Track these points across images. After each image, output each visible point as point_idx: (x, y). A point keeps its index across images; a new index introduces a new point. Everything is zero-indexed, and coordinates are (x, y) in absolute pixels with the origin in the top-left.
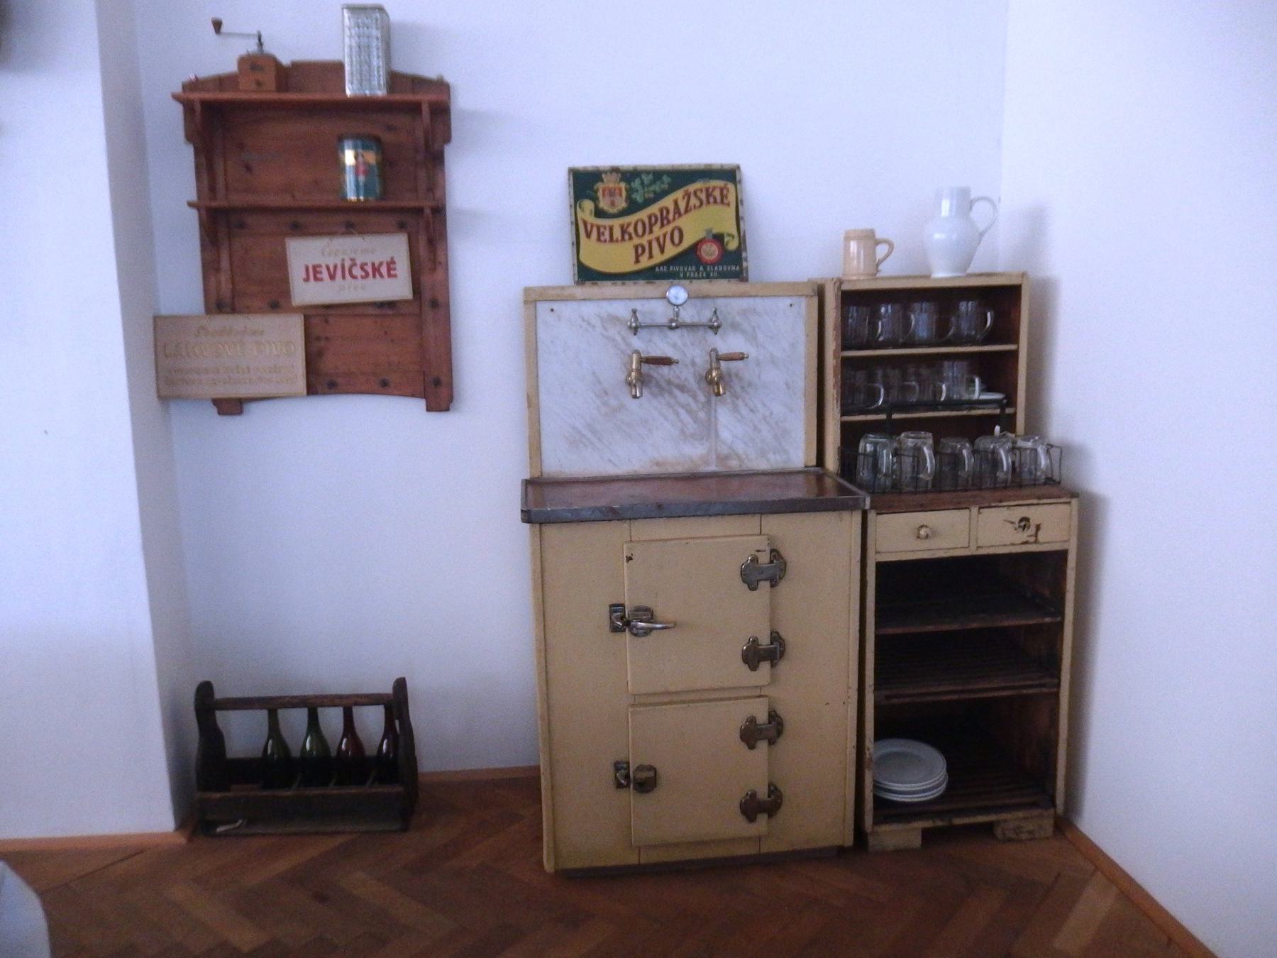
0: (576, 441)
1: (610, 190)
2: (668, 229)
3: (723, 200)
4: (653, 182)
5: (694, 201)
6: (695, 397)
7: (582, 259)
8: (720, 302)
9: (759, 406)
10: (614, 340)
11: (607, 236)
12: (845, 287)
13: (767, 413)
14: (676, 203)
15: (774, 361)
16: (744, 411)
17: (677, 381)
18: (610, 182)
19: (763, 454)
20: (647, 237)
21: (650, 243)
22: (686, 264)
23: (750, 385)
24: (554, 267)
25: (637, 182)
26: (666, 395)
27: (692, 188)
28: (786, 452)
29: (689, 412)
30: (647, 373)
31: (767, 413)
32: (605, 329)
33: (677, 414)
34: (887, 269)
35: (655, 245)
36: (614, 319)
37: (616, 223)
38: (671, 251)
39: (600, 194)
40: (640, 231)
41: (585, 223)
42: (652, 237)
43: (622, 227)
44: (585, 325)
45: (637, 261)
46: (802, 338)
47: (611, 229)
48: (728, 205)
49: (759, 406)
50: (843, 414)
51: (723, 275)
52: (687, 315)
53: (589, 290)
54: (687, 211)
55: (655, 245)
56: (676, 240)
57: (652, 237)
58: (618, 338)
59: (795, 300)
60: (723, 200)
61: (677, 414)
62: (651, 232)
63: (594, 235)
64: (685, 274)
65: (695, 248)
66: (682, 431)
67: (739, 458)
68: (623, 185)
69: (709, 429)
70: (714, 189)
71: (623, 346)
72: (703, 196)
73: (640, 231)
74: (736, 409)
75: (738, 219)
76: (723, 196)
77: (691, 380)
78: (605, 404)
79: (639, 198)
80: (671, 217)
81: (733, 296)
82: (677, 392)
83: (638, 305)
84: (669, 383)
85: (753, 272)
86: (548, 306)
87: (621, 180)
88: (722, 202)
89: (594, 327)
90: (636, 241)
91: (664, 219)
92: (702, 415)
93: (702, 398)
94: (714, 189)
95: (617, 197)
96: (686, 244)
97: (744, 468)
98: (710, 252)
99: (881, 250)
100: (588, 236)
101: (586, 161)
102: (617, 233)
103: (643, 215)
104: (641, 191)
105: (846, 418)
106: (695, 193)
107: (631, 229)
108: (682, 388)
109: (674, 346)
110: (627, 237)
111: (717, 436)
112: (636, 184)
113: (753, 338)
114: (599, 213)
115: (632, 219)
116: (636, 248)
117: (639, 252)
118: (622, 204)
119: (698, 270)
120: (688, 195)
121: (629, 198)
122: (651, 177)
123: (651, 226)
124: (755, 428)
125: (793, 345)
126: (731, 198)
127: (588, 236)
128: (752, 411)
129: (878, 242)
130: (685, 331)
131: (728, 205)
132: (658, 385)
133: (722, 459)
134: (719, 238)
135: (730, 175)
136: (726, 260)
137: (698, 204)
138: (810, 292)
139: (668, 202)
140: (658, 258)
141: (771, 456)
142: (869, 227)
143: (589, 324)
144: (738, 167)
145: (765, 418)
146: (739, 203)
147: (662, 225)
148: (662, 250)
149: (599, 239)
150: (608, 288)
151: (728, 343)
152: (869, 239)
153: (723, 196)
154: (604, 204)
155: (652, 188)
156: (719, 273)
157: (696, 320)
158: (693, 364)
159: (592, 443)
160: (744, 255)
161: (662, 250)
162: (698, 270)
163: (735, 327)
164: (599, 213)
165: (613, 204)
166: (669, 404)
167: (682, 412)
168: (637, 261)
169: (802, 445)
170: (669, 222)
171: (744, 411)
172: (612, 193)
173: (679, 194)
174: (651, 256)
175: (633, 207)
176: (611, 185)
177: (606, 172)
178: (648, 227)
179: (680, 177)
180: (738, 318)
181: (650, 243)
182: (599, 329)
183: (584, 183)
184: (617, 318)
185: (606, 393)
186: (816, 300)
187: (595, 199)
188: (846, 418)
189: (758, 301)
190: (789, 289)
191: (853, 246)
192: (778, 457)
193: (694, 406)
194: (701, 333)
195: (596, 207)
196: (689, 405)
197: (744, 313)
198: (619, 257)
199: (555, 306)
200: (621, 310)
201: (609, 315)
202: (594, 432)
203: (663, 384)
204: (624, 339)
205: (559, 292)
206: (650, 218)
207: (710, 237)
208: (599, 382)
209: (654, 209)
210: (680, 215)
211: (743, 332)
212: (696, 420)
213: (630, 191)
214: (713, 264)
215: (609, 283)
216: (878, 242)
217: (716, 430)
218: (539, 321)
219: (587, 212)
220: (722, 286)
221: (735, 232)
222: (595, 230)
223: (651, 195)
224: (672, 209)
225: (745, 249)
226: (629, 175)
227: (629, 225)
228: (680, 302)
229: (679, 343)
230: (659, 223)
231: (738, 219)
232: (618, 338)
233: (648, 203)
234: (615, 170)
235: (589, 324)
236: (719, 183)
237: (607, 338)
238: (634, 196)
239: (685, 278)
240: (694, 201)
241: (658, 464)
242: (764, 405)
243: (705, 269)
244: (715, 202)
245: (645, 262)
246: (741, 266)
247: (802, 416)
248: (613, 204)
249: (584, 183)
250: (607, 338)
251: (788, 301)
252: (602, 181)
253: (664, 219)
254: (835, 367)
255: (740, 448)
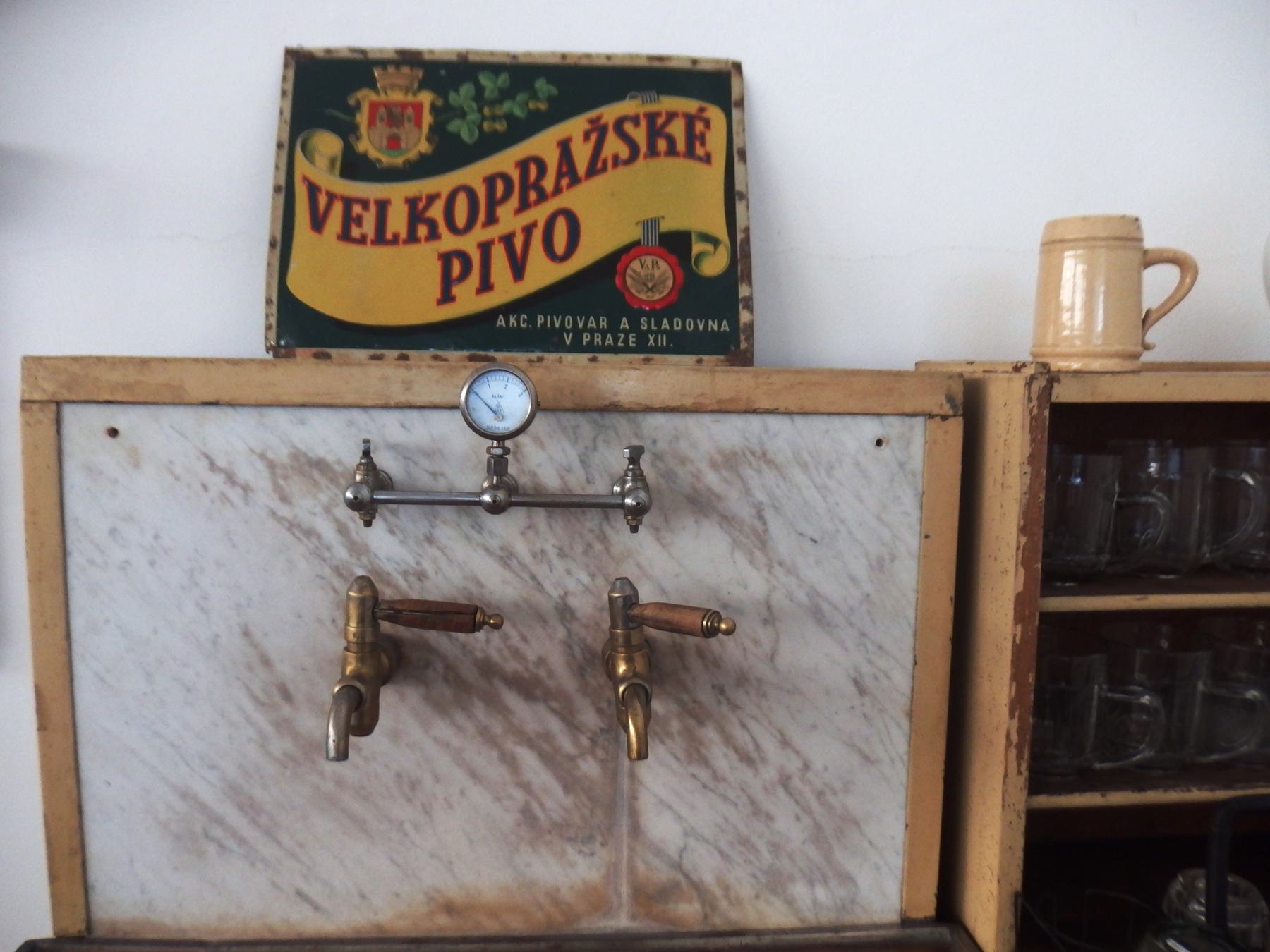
0: (196, 833)
1: (388, 106)
2: (539, 214)
3: (693, 146)
4: (506, 94)
5: (613, 146)
6: (569, 719)
7: (291, 284)
8: (656, 424)
9: (770, 747)
10: (310, 533)
11: (369, 227)
12: (1065, 393)
13: (793, 765)
14: (565, 146)
15: (818, 614)
16: (721, 757)
17: (512, 666)
18: (393, 90)
19: (775, 883)
20: (480, 234)
21: (485, 248)
22: (587, 309)
23: (742, 679)
24: (221, 311)
25: (467, 90)
26: (480, 710)
27: (610, 113)
28: (847, 879)
29: (550, 759)
30: (399, 648)
31: (793, 765)
32: (284, 499)
33: (510, 762)
34: (1166, 341)
35: (499, 253)
36: (312, 467)
37: (397, 193)
38: (543, 273)
39: (362, 118)
40: (461, 217)
41: (313, 190)
42: (494, 232)
43: (412, 202)
44: (217, 480)
45: (447, 297)
46: (911, 541)
47: (383, 206)
48: (707, 159)
49: (770, 747)
50: (1036, 784)
51: (680, 344)
52: (547, 461)
53: (305, 372)
54: (592, 171)
55: (499, 253)
56: (560, 244)
57: (494, 232)
58: (327, 530)
59: (892, 427)
60: (693, 146)
61: (510, 762)
62: (492, 220)
63: (334, 223)
64: (578, 333)
65: (610, 265)
66: (527, 815)
67: (699, 889)
68: (426, 98)
69: (607, 813)
70: (671, 116)
71: (341, 553)
72: (640, 134)
73: (461, 217)
74: (696, 753)
75: (732, 196)
76: (693, 138)
77: (557, 660)
78: (284, 726)
79: (464, 130)
80: (548, 184)
81: (696, 409)
82: (512, 700)
83: (390, 429)
84: (488, 669)
85: (769, 334)
86: (100, 417)
87: (423, 85)
88: (690, 153)
89: (246, 489)
90: (449, 242)
91: (529, 184)
92: (590, 768)
93: (590, 718)
94: (671, 116)
95: (408, 126)
96: (588, 254)
97: (718, 922)
98: (651, 278)
99: (1158, 283)
100: (318, 224)
101: (330, 34)
102: (397, 221)
103: (473, 175)
104: (473, 117)
105: (1044, 801)
106: (619, 124)
107: (436, 212)
108: (528, 687)
109: (506, 557)
110: (422, 231)
111: (636, 831)
112: (463, 95)
113: (754, 537)
114: (354, 166)
115: (443, 184)
116: (446, 258)
117: (453, 269)
118: (419, 145)
119: (614, 328)
120: (598, 130)
121: (438, 130)
122: (503, 79)
123: (493, 203)
124: (757, 811)
125: (879, 566)
126: (716, 141)
127: (318, 224)
128: (746, 759)
129: (1150, 259)
130: (540, 515)
131: (707, 159)
132: (453, 677)
133: (648, 896)
134: (676, 245)
135: (716, 85)
136: (697, 302)
137: (624, 152)
138: (937, 403)
139: (544, 144)
140: (506, 290)
141: (799, 890)
142: (1132, 212)
143: (231, 478)
144: (737, 66)
145: (785, 781)
146: (735, 155)
147: (524, 206)
148: (518, 271)
149: (345, 236)
150: (358, 371)
151: (677, 564)
152: (1123, 247)
153: (693, 138)
154: (366, 145)
155: (507, 106)
156: (671, 334)
157: (577, 484)
158: (565, 612)
159: (242, 841)
160: (743, 291)
161: (518, 271)
162: (614, 328)
163: (701, 504)
164: (354, 166)
165: (394, 143)
166: (486, 735)
167: (528, 759)
168: (447, 297)
169: (896, 861)
170: (543, 197)
171: (721, 757)
172: (394, 116)
173: (575, 127)
174: (486, 285)
175: (448, 153)
176: (397, 96)
177: (383, 63)
178: (485, 207)
179: (582, 84)
180: (712, 479)
181: (485, 248)
182: (264, 496)
183: (322, 88)
184: (320, 465)
185: (287, 695)
186: (956, 427)
187: (347, 131)
188: (1044, 801)
189: (775, 423)
190: (870, 392)
191: (1072, 270)
192: (821, 894)
193: (565, 743)
194: (592, 520)
195: (348, 150)
196: (547, 736)
197: (730, 461)
198: (402, 284)
199: (123, 418)
200: (332, 438)
201: (297, 455)
202: (250, 808)
203: (469, 673)
204: (342, 530)
205: (132, 375)
206: (490, 181)
207: (654, 241)
208: (266, 662)
209: (505, 161)
210: (575, 180)
211: (727, 520)
212: (570, 783)
213: (443, 113)
214: (658, 313)
215: (361, 354)
216: (1150, 259)
217: (634, 814)
218: (70, 466)
219: (322, 162)
220: (671, 377)
221: (723, 234)
222: (338, 208)
223: (500, 127)
224: (553, 160)
225: (748, 277)
226: (446, 74)
227: (432, 198)
228: (511, 424)
229: (521, 548)
230: (514, 202)
231: (732, 196)
232: (327, 530)
233: (490, 145)
234: (408, 58)
235: (231, 478)
236: (689, 105)
237: (293, 526)
238: (454, 126)
239: (577, 347)
240: (613, 146)
241: (450, 908)
242: (785, 743)
243: (635, 326)
244: (672, 151)
245: (468, 301)
246: (734, 320)
247: (899, 774)
248: (394, 143)
249: (322, 88)
250: (293, 526)
251: (870, 428)
252: (372, 84)
253: (529, 184)
254: (1017, 651)
255: (706, 867)
